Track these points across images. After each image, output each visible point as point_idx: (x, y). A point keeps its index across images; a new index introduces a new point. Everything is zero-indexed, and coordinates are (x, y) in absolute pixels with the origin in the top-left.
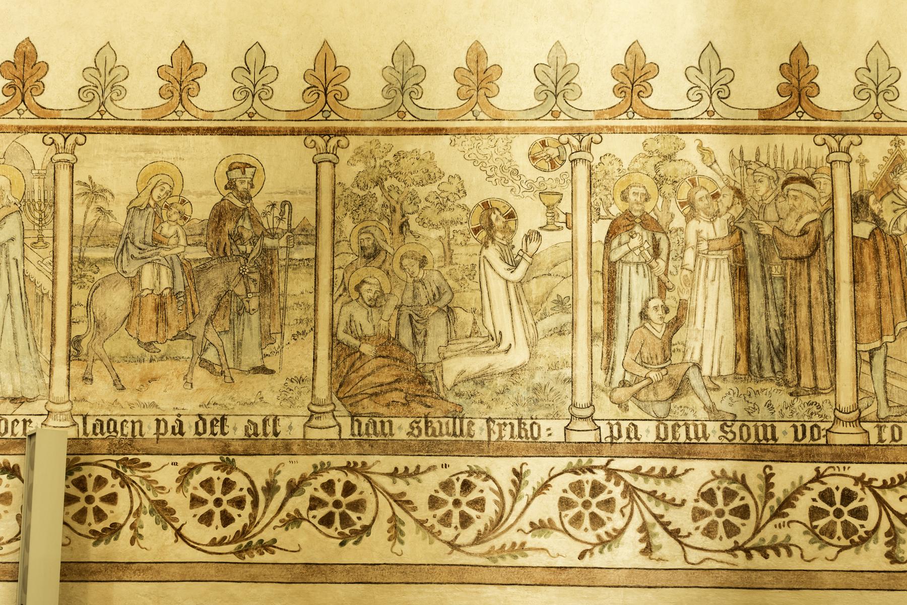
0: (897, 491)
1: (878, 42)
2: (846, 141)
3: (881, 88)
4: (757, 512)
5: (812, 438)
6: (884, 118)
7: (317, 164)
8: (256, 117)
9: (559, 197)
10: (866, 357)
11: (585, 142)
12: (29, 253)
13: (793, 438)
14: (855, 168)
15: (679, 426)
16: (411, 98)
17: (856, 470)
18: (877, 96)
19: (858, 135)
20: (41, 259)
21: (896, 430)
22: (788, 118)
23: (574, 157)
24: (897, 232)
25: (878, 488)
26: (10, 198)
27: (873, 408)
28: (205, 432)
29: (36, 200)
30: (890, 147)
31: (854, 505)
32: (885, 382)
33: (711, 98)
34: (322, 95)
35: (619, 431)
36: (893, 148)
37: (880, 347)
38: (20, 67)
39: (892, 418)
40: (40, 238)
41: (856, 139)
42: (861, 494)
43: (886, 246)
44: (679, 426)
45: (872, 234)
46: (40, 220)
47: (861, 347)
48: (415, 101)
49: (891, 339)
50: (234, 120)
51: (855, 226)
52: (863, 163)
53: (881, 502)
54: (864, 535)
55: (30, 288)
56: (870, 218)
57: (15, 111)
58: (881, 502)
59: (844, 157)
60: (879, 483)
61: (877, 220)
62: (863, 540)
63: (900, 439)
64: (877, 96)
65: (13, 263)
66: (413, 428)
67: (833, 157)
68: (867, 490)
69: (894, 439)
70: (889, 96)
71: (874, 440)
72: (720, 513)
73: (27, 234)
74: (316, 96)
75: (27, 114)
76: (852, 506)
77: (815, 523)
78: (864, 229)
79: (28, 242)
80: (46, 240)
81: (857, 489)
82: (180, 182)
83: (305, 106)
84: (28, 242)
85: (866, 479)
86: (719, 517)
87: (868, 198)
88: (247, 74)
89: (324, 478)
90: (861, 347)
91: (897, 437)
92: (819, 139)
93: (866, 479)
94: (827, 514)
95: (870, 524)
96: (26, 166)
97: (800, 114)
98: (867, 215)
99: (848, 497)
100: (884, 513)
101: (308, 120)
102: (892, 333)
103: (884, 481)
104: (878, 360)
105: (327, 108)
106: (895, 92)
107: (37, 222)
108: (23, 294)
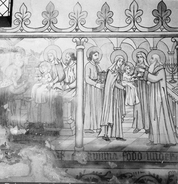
1: (51, 1)
2: (83, 40)
5: (138, 159)
8: (23, 31)
9: (58, 64)
12: (169, 85)
16: (166, 23)
20: (174, 88)
22: (101, 31)
26: (160, 63)
28: (136, 158)
29: (170, 64)
33: (105, 24)
38: (160, 12)
40: (173, 79)
46: (172, 71)
48: (27, 26)
50: (71, 32)
55: (170, 99)
57: (103, 30)
65: (162, 89)
73: (167, 78)
74: (18, 23)
75: (164, 30)
79: (168, 80)
80: (175, 80)
82: (126, 57)
84: (168, 80)
91: (140, 158)
92: (74, 40)
96: (166, 51)
97: (49, 30)
101: (71, 32)
105: (134, 27)
106: (112, 20)
107: (171, 73)
108: (168, 102)
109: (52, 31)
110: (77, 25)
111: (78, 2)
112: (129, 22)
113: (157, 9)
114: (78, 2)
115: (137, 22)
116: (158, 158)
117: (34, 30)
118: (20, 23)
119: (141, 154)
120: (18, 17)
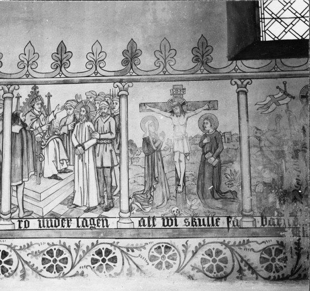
0: (26, 252)
2: (12, 88)
3: (30, 63)
4: (72, 261)
6: (30, 77)
7: (238, 93)
10: (15, 188)
11: (245, 83)
13: (38, 226)
14: (15, 100)
15: (100, 220)
17: (8, 242)
18: (28, 67)
19: (18, 85)
21: (27, 222)
23: (120, 94)
24: (32, 130)
25: (18, 250)
27: (17, 212)
28: (266, 224)
30: (31, 90)
31: (111, 256)
32: (23, 200)
34: (26, 67)
35: (52, 223)
36: (33, 90)
37: (22, 184)
39: (25, 217)
41: (17, 87)
42: (10, 253)
43: (27, 136)
44: (100, 220)
45: (21, 131)
47: (13, 184)
48: (103, 68)
49: (27, 179)
50: (19, 78)
51: (13, 127)
52: (18, 97)
53: (19, 257)
54: (11, 273)
56: (20, 123)
58: (19, 257)
59: (10, 95)
60: (19, 248)
61: (24, 125)
62: (10, 275)
63: (28, 226)
64: (28, 67)
66: (186, 223)
67: (5, 96)
68: (13, 251)
69: (25, 227)
70: (33, 67)
71: (17, 227)
72: (55, 261)
76: (49, 258)
77: (204, 266)
78: (17, 128)
81: (8, 250)
83: (156, 68)
85: (13, 246)
86: (275, 262)
87: (19, 114)
88: (161, 55)
89: (206, 248)
90: (13, 184)
93: (13, 246)
94: (60, 261)
95: (13, 267)
98: (18, 122)
99: (108, 252)
100: (20, 261)
102: (27, 176)
103: (21, 247)
104: (21, 189)
105: (276, 66)
106: (36, 65)
109: (239, 71)
110: (165, 67)
111: (30, 42)
112: (22, 66)
113: (159, 50)
114: (30, 42)
115: (100, 67)
116: (53, 225)
117: (182, 73)
118: (94, 65)
119: (107, 221)
120: (22, 59)
